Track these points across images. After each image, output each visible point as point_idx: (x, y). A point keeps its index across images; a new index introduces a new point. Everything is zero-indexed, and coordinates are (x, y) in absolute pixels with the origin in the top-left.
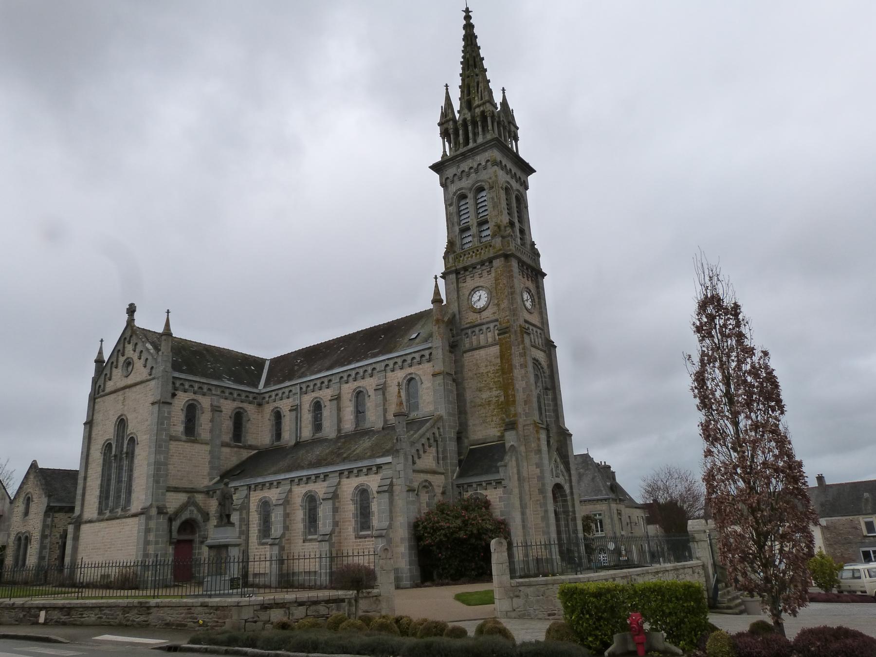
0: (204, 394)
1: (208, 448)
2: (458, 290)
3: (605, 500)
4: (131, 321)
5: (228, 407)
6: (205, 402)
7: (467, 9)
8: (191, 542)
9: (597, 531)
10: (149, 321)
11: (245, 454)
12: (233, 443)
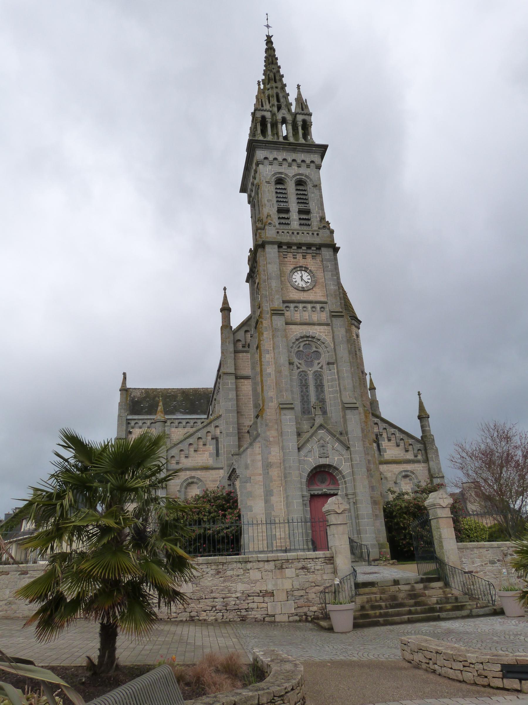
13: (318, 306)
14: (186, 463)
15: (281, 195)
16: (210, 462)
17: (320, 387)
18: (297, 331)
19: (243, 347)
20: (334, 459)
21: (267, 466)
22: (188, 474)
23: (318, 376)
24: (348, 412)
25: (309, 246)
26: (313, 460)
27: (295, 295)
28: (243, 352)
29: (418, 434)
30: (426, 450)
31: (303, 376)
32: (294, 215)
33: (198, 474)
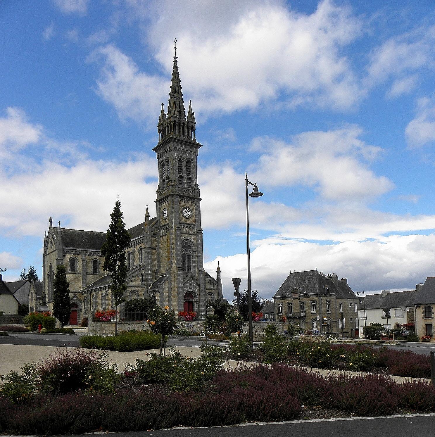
0: (78, 254)
1: (81, 275)
2: (160, 208)
3: (318, 295)
4: (51, 225)
5: (90, 259)
6: (79, 258)
7: (175, 56)
8: (77, 311)
9: (313, 311)
10: (55, 225)
11: (99, 278)
12: (92, 273)
13: (192, 226)
14: (131, 284)
15: (180, 167)
16: (140, 284)
17: (189, 260)
18: (184, 236)
19: (154, 235)
20: (194, 289)
21: (170, 290)
22: (132, 289)
23: (189, 256)
24: (200, 272)
25: (191, 198)
26: (187, 289)
27: (184, 221)
28: (154, 237)
29: (216, 279)
30: (218, 285)
31: (184, 255)
32: (185, 180)
33: (136, 289)
